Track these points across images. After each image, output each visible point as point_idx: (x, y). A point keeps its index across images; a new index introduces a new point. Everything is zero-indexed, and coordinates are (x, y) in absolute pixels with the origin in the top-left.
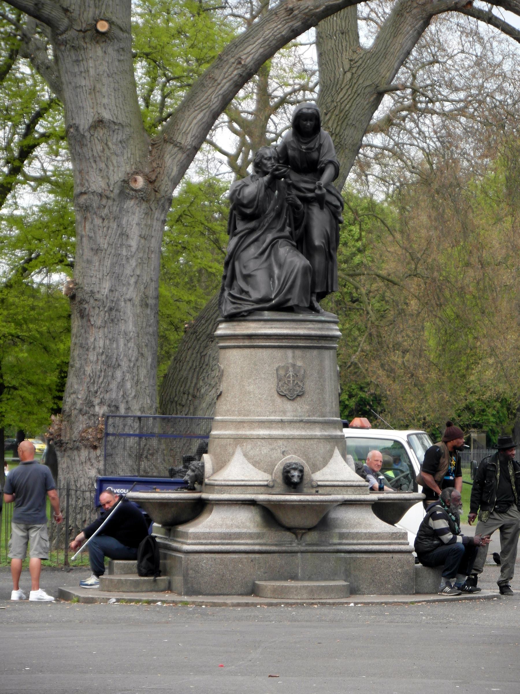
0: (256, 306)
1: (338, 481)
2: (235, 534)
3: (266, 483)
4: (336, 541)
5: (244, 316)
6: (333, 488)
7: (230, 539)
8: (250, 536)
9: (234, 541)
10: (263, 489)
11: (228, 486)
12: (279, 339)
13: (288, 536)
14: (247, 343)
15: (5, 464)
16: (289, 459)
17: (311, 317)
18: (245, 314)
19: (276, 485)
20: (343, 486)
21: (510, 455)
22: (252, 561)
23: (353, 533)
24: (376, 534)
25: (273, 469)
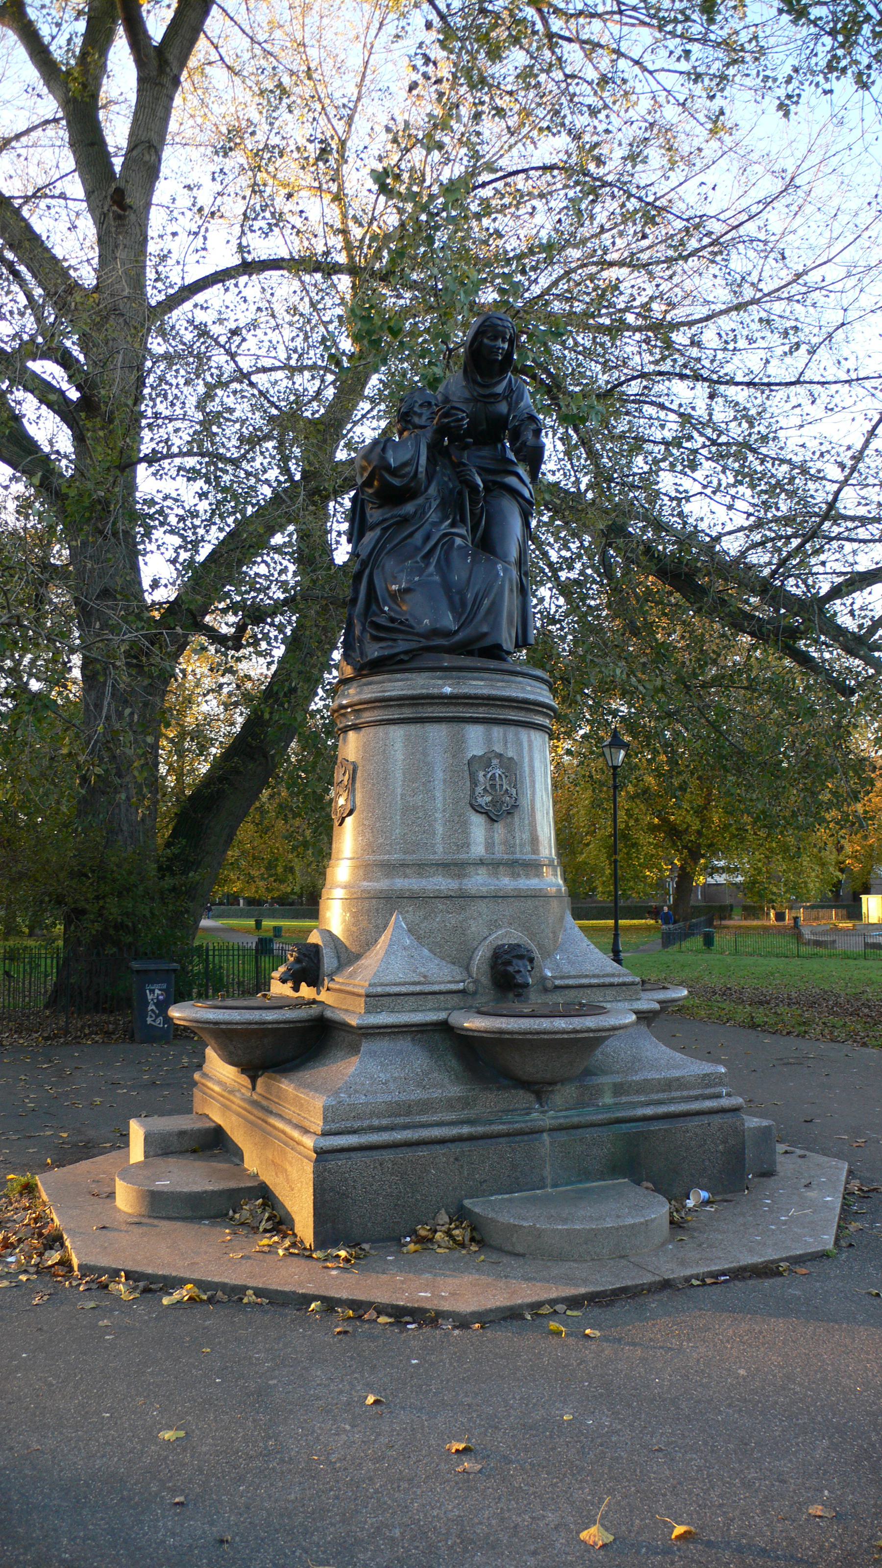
0: (424, 643)
1: (586, 976)
2: (418, 1102)
3: (461, 986)
4: (608, 1100)
5: (402, 662)
6: (582, 991)
7: (408, 1113)
8: (450, 1104)
9: (418, 1119)
10: (455, 1000)
11: (389, 995)
12: (472, 705)
13: (522, 1098)
14: (408, 713)
15: (79, 638)
16: (504, 936)
17: (478, 686)
18: (406, 658)
19: (481, 990)
20: (599, 986)
21: (195, 1084)
22: (456, 1159)
23: (637, 1083)
24: (678, 1079)
25: (471, 958)
